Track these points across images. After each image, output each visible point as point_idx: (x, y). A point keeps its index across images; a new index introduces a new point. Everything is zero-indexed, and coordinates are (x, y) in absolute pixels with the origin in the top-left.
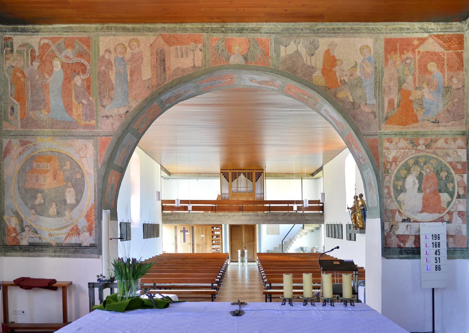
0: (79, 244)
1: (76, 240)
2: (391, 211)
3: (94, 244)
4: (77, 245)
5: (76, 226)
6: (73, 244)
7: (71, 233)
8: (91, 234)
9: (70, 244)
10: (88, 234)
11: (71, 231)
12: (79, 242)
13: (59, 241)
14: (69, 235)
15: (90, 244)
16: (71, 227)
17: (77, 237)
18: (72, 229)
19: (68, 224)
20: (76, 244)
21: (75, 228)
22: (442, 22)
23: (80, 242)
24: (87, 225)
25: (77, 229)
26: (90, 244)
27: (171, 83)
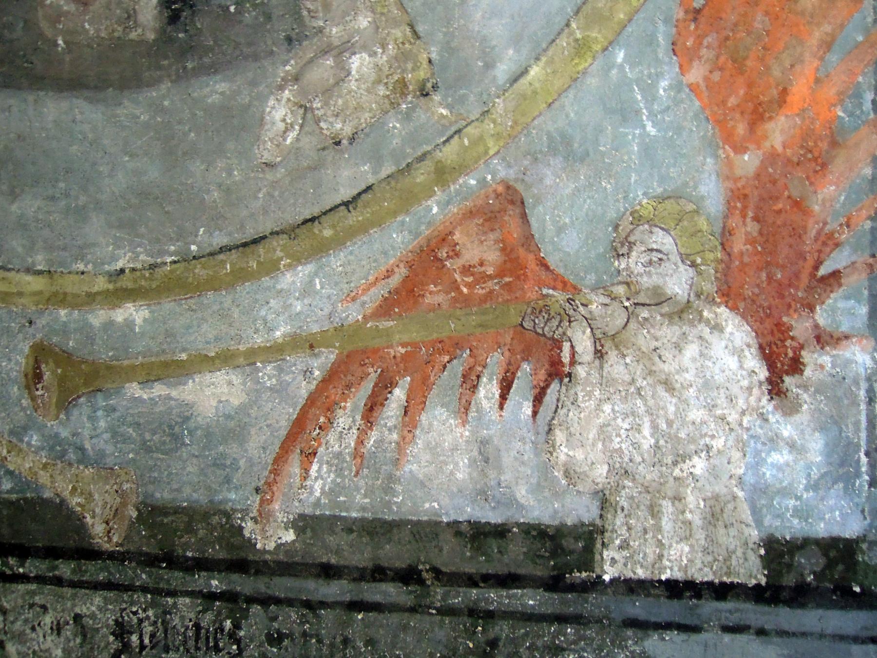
0: (547, 538)
1: (485, 455)
2: (826, 555)
3: (841, 552)
4: (513, 556)
5: (507, 205)
6: (427, 531)
7: (400, 335)
8: (781, 365)
9: (376, 529)
10: (729, 350)
11: (404, 298)
12: (535, 507)
13: (184, 482)
14: (362, 369)
15: (777, 552)
16: (397, 240)
17: (503, 416)
18: (429, 260)
19: (347, 177)
20: (480, 535)
21: (479, 250)
22: (219, 560)
23: (578, 510)
24: (711, 192)
25: (521, 261)
26: (777, 552)
27: (330, 409)
